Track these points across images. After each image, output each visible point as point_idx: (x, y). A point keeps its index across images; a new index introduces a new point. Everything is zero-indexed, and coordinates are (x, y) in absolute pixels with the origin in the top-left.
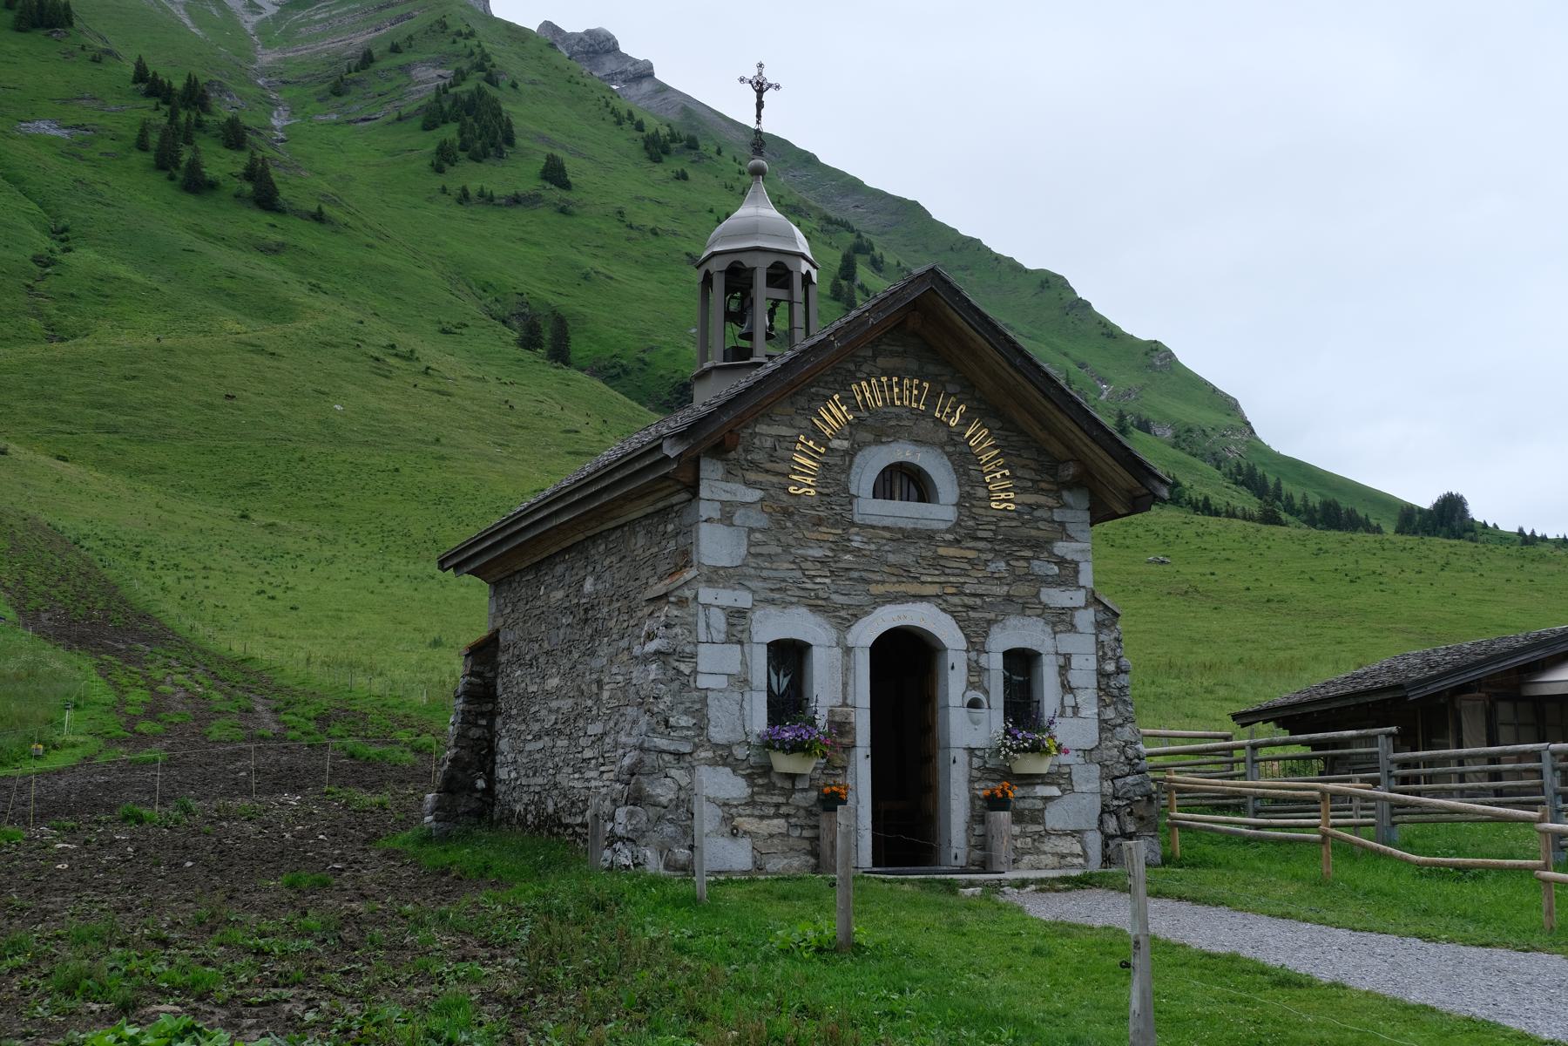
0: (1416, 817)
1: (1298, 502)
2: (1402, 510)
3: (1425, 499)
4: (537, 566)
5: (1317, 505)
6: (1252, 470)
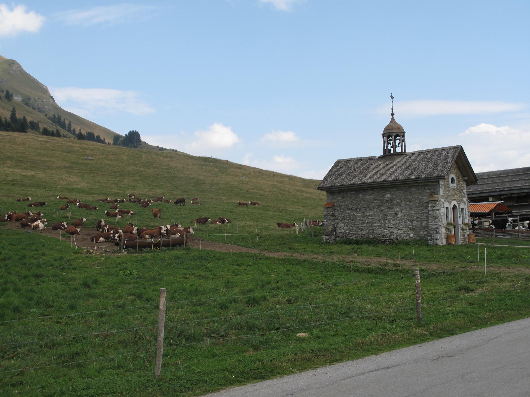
0: (503, 208)
1: (77, 132)
2: (115, 136)
3: (123, 132)
4: (423, 186)
5: (85, 134)
6: (59, 118)
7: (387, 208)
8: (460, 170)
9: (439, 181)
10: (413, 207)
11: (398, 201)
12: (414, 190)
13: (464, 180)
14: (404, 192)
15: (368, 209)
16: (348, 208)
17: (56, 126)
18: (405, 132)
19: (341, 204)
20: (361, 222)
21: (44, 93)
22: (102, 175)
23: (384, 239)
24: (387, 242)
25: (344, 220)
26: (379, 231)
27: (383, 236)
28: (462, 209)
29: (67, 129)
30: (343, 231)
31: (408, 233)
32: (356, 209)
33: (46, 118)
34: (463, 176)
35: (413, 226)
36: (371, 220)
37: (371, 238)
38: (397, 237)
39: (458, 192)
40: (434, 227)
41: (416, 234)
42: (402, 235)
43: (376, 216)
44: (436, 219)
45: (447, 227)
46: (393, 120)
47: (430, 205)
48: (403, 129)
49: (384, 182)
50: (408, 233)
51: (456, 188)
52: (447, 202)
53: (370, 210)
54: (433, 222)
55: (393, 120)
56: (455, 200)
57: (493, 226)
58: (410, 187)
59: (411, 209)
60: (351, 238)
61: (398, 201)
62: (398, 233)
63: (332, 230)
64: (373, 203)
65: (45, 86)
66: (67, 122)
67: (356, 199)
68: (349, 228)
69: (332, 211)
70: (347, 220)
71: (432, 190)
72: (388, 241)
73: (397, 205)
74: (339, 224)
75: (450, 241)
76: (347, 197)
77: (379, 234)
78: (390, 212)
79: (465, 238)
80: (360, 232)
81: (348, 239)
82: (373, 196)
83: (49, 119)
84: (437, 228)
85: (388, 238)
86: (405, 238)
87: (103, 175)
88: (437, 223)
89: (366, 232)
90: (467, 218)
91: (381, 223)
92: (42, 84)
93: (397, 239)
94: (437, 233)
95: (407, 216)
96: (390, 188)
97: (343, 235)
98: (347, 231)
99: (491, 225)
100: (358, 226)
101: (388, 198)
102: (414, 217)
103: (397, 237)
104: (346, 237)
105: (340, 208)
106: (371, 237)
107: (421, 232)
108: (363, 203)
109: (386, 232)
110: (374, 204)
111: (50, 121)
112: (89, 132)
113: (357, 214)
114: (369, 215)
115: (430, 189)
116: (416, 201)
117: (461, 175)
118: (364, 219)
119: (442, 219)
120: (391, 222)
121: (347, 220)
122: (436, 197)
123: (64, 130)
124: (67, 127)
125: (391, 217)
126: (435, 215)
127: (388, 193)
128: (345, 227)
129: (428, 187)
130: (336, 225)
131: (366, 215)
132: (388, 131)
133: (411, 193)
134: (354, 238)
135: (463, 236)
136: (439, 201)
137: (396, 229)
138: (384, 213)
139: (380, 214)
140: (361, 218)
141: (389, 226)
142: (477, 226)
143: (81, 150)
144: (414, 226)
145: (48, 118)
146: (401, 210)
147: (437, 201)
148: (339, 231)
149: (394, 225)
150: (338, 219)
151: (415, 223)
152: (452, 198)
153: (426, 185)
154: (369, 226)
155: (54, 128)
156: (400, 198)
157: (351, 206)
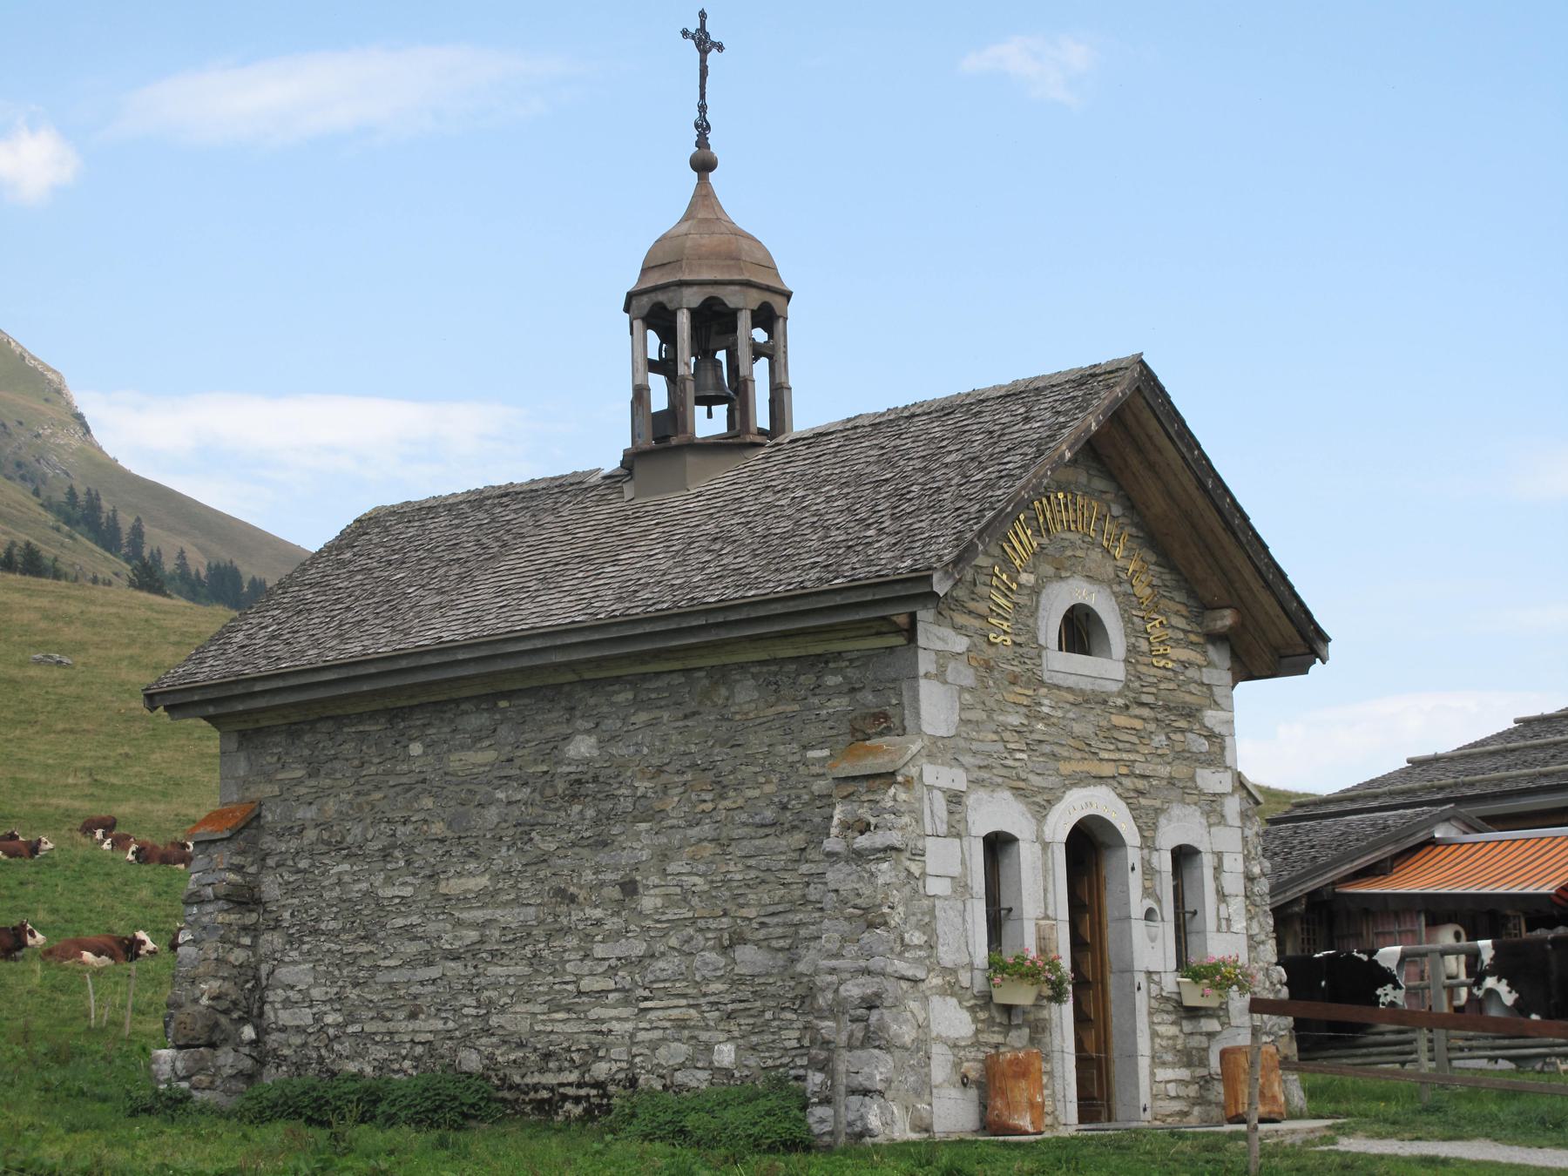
5: (203, 573)
6: (93, 504)
7: (574, 845)
8: (1165, 558)
9: (913, 618)
10: (742, 831)
11: (642, 786)
12: (745, 695)
13: (1214, 638)
14: (686, 717)
15: (457, 851)
16: (339, 847)
17: (71, 537)
18: (789, 283)
19: (306, 813)
20: (412, 948)
21: (47, 400)
22: (64, 731)
23: (550, 1079)
24: (568, 1106)
25: (315, 932)
26: (517, 1019)
27: (547, 1056)
28: (1183, 856)
29: (125, 550)
30: (305, 1017)
31: (704, 1036)
32: (386, 855)
33: (33, 504)
34: (1202, 607)
35: (737, 981)
36: (473, 935)
37: (470, 1075)
38: (632, 1064)
39: (1138, 724)
40: (854, 990)
41: (753, 1048)
42: (662, 1051)
43: (506, 904)
44: (871, 925)
45: (986, 1000)
46: (704, 196)
47: (838, 814)
48: (771, 269)
49: (539, 644)
50: (704, 1036)
51: (1115, 687)
52: (1007, 794)
53: (471, 854)
54: (851, 949)
55: (704, 196)
56: (1100, 779)
57: (1503, 988)
58: (721, 675)
59: (723, 843)
60: (352, 1067)
61: (642, 786)
62: (641, 1036)
63: (224, 1004)
64: (493, 802)
65: (55, 372)
66: (126, 522)
67: (386, 773)
68: (339, 998)
69: (238, 869)
70: (333, 935)
71: (869, 697)
72: (577, 1100)
73: (636, 820)
74: (281, 961)
75: (999, 1103)
76: (337, 765)
77: (521, 1045)
78: (588, 876)
79: (1205, 1082)
80: (403, 1026)
81: (333, 1074)
82: (491, 755)
83: (48, 506)
84: (870, 1004)
85: (573, 1077)
86: (680, 1077)
87: (72, 731)
88: (877, 963)
89: (439, 1025)
90: (1239, 925)
91: (536, 959)
92: (41, 363)
93: (633, 1082)
94: (872, 1039)
95: (695, 901)
96: (594, 685)
97: (305, 1045)
98: (329, 1019)
99: (1490, 982)
100: (395, 976)
101: (578, 762)
102: (745, 912)
103: (632, 1064)
104: (321, 1060)
105: (294, 844)
106: (471, 1061)
107: (785, 1034)
108: (428, 802)
109: (563, 1027)
110: (492, 814)
111: (50, 518)
112: (218, 567)
113: (389, 892)
114: (463, 900)
115: (853, 690)
116: (759, 785)
117: (1179, 596)
118: (432, 928)
119: (928, 928)
120: (599, 951)
121: (333, 935)
122: (883, 753)
123: (108, 555)
124: (124, 541)
125: (598, 913)
126: (867, 891)
127: (580, 724)
128: (316, 984)
129: (835, 672)
130: (264, 969)
131: (447, 898)
132: (656, 279)
133: (726, 725)
134: (368, 1070)
135: (1189, 1065)
136: (908, 783)
137: (626, 1002)
138: (555, 882)
139: (526, 885)
140: (415, 920)
141: (586, 984)
142: (1397, 986)
143: (43, 625)
144: (740, 980)
145: (42, 505)
146: (664, 856)
147: (889, 777)
148: (285, 1017)
149: (612, 971)
150: (277, 926)
151: (749, 957)
152: (1067, 768)
153: (823, 660)
154: (460, 977)
155: (62, 545)
156: (656, 762)
157: (357, 830)
